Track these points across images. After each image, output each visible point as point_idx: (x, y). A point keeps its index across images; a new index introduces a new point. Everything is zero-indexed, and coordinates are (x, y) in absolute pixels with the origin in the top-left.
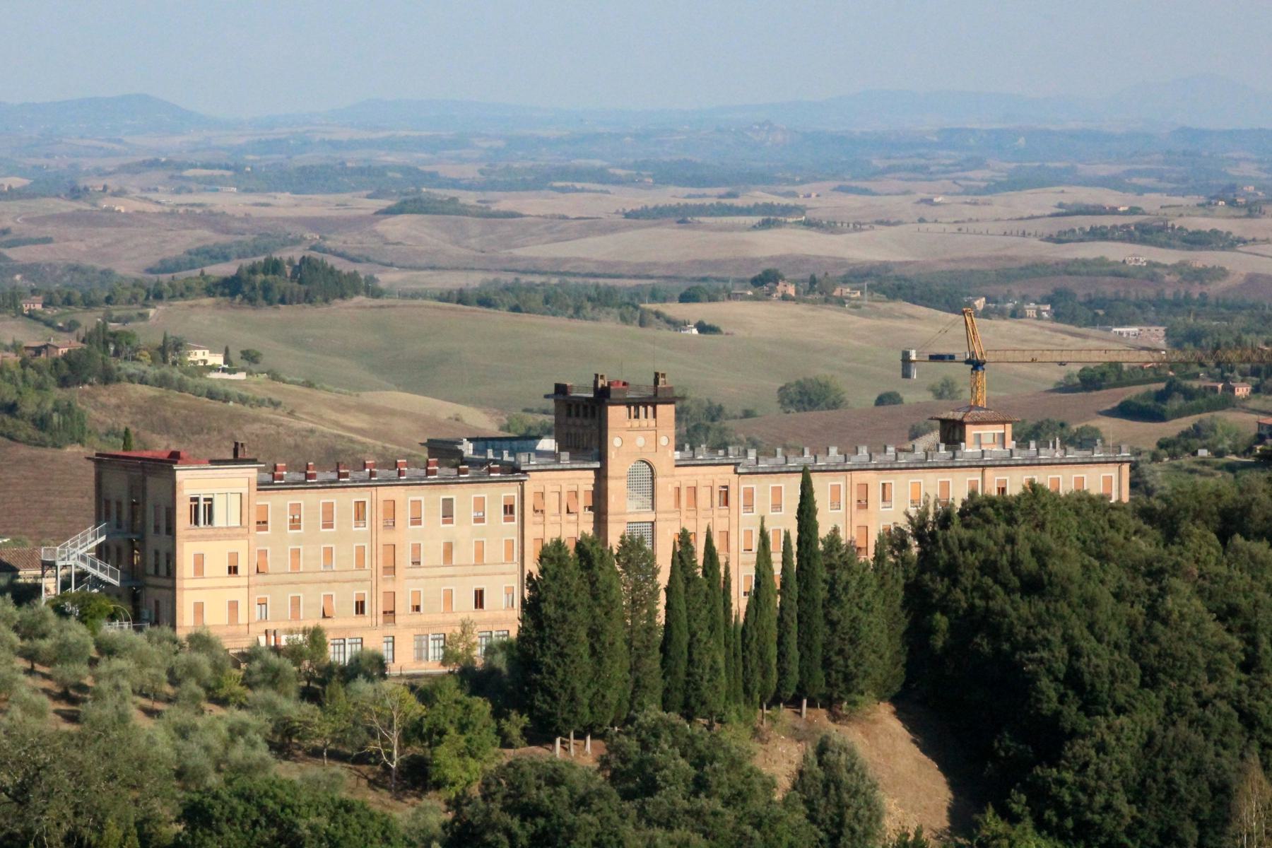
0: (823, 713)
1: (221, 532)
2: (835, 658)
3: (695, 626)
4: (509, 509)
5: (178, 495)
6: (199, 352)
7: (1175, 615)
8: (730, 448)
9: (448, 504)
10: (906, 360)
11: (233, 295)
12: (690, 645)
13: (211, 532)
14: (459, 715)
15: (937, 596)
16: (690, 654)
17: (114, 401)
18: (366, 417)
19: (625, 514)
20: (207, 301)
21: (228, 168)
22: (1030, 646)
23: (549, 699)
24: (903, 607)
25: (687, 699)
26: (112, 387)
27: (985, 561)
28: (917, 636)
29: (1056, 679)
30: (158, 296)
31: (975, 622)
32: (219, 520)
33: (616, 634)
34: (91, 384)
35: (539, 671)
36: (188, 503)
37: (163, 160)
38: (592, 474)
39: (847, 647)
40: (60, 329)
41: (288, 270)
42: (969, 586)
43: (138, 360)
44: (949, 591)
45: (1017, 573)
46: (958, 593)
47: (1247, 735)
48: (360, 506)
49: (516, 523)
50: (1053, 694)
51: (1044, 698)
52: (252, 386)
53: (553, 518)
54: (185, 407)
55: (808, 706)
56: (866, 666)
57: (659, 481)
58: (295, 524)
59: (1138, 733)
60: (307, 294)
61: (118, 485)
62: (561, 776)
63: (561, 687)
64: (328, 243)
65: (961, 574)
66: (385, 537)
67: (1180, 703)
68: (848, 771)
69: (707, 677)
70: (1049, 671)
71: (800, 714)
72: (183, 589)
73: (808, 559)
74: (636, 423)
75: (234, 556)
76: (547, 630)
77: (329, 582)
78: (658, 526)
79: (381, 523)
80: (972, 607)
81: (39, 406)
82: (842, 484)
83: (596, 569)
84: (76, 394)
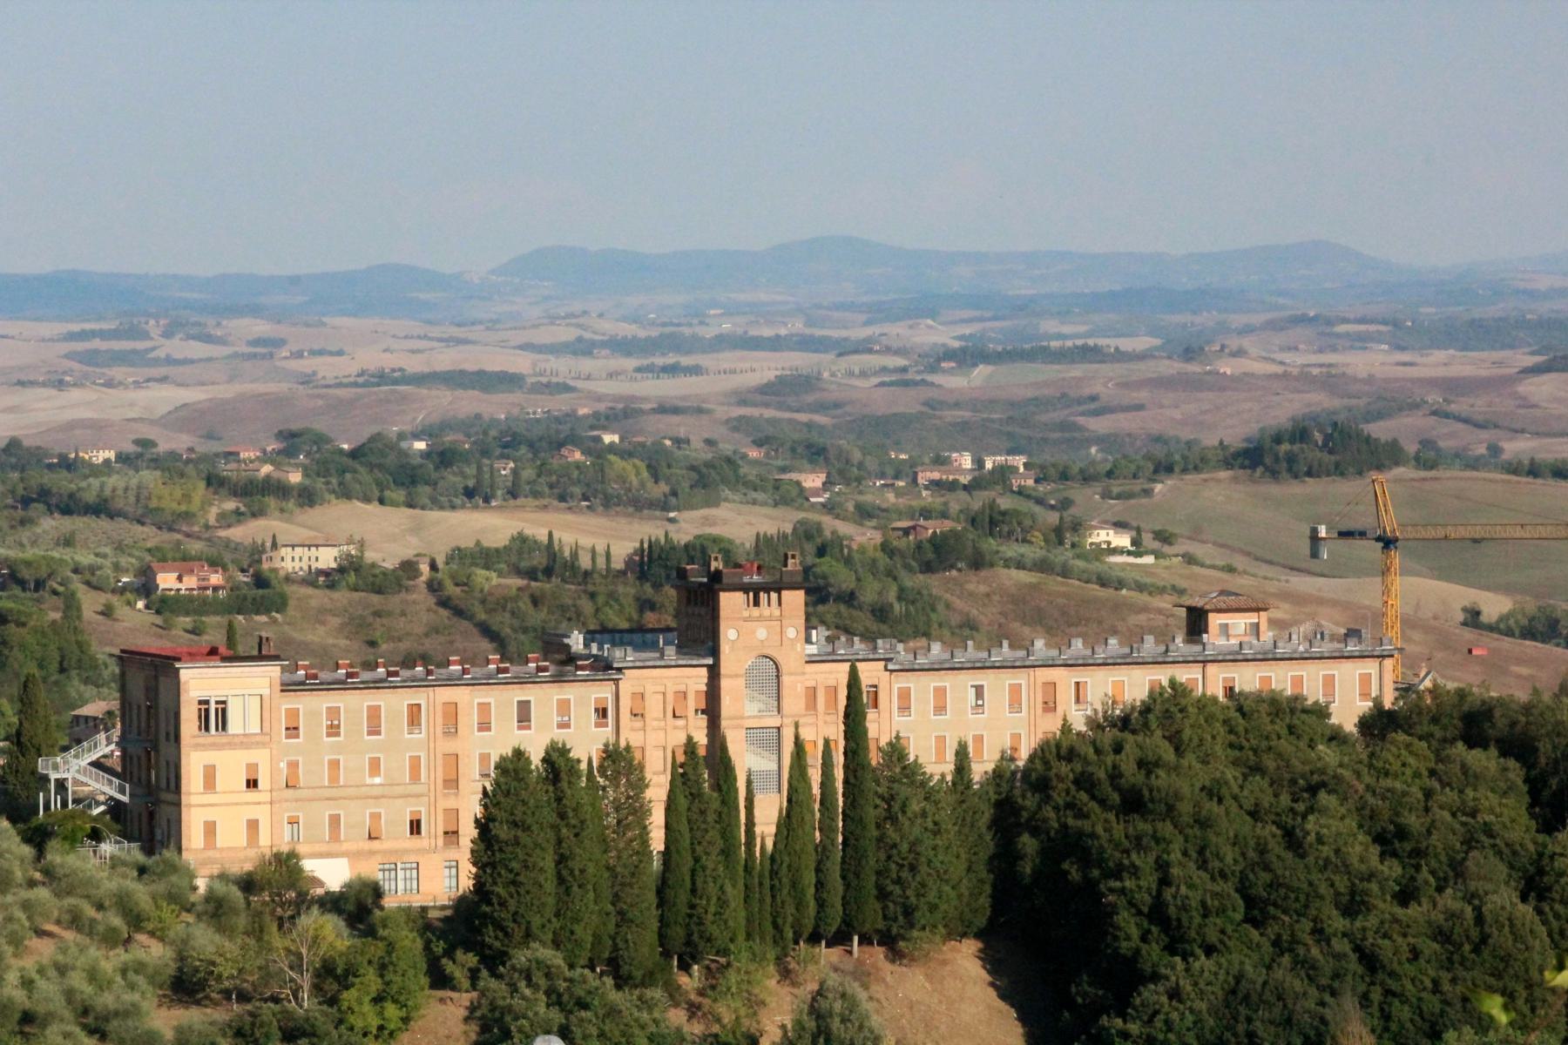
0: (879, 952)
1: (236, 740)
2: (890, 888)
3: (699, 849)
4: (602, 713)
5: (183, 698)
6: (1103, 533)
7: (1312, 838)
8: (880, 642)
9: (524, 707)
10: (1315, 538)
11: (1253, 467)
12: (693, 872)
13: (224, 740)
14: (380, 953)
15: (1025, 814)
16: (693, 883)
17: (983, 589)
18: (1286, 606)
20: (1224, 474)
21: (1384, 322)
22: (1117, 874)
23: (500, 935)
24: (989, 828)
25: (690, 935)
26: (983, 573)
27: (1083, 773)
28: (1004, 858)
29: (1140, 913)
30: (1169, 469)
31: (1069, 845)
32: (234, 726)
33: (587, 858)
34: (960, 570)
35: (490, 903)
36: (195, 707)
37: (1312, 314)
38: (704, 671)
39: (905, 874)
40: (1052, 507)
41: (1318, 437)
42: (1061, 802)
43: (1030, 542)
44: (1040, 808)
45: (1116, 788)
46: (1049, 812)
47: (1367, 979)
48: (414, 710)
50: (1135, 932)
51: (1121, 934)
52: (1159, 571)
53: (655, 723)
54: (1064, 595)
55: (860, 943)
56: (932, 896)
57: (785, 679)
58: (333, 730)
59: (1221, 978)
60: (1337, 465)
61: (137, 682)
62: (313, 1026)
63: (515, 921)
64: (1453, 407)
65: (1053, 788)
66: (450, 746)
67: (1291, 943)
68: (843, 1021)
69: (712, 909)
70: (1131, 904)
71: (850, 953)
72: (190, 806)
74: (755, 612)
75: (252, 767)
77: (376, 798)
79: (439, 730)
80: (1065, 826)
81: (880, 593)
83: (564, 784)
84: (933, 584)
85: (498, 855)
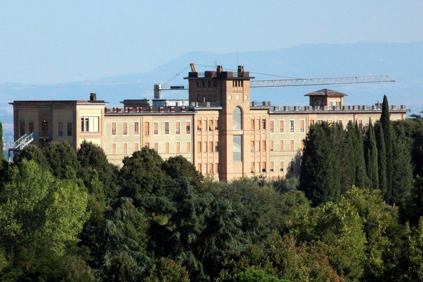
4: (188, 128)
5: (77, 117)
19: (233, 131)
32: (91, 129)
35: (315, 181)
38: (217, 112)
49: (190, 135)
57: (245, 116)
58: (114, 132)
73: (387, 137)
74: (236, 89)
76: (319, 162)
78: (245, 136)
82: (304, 120)
85: (357, 247)
